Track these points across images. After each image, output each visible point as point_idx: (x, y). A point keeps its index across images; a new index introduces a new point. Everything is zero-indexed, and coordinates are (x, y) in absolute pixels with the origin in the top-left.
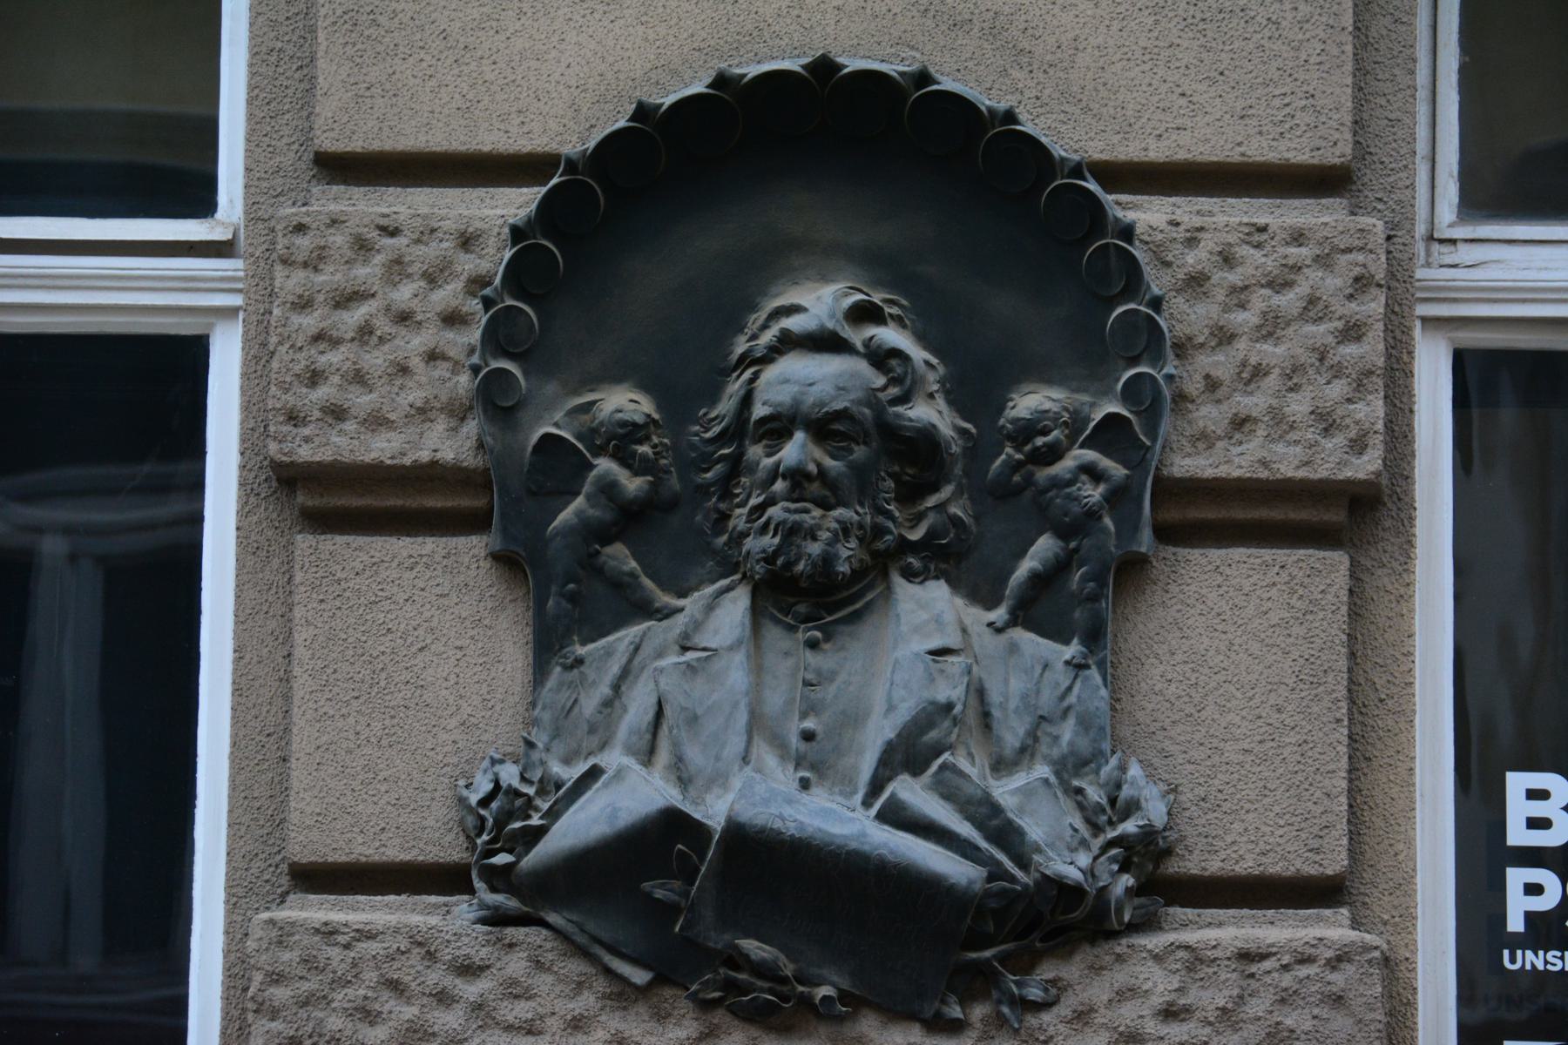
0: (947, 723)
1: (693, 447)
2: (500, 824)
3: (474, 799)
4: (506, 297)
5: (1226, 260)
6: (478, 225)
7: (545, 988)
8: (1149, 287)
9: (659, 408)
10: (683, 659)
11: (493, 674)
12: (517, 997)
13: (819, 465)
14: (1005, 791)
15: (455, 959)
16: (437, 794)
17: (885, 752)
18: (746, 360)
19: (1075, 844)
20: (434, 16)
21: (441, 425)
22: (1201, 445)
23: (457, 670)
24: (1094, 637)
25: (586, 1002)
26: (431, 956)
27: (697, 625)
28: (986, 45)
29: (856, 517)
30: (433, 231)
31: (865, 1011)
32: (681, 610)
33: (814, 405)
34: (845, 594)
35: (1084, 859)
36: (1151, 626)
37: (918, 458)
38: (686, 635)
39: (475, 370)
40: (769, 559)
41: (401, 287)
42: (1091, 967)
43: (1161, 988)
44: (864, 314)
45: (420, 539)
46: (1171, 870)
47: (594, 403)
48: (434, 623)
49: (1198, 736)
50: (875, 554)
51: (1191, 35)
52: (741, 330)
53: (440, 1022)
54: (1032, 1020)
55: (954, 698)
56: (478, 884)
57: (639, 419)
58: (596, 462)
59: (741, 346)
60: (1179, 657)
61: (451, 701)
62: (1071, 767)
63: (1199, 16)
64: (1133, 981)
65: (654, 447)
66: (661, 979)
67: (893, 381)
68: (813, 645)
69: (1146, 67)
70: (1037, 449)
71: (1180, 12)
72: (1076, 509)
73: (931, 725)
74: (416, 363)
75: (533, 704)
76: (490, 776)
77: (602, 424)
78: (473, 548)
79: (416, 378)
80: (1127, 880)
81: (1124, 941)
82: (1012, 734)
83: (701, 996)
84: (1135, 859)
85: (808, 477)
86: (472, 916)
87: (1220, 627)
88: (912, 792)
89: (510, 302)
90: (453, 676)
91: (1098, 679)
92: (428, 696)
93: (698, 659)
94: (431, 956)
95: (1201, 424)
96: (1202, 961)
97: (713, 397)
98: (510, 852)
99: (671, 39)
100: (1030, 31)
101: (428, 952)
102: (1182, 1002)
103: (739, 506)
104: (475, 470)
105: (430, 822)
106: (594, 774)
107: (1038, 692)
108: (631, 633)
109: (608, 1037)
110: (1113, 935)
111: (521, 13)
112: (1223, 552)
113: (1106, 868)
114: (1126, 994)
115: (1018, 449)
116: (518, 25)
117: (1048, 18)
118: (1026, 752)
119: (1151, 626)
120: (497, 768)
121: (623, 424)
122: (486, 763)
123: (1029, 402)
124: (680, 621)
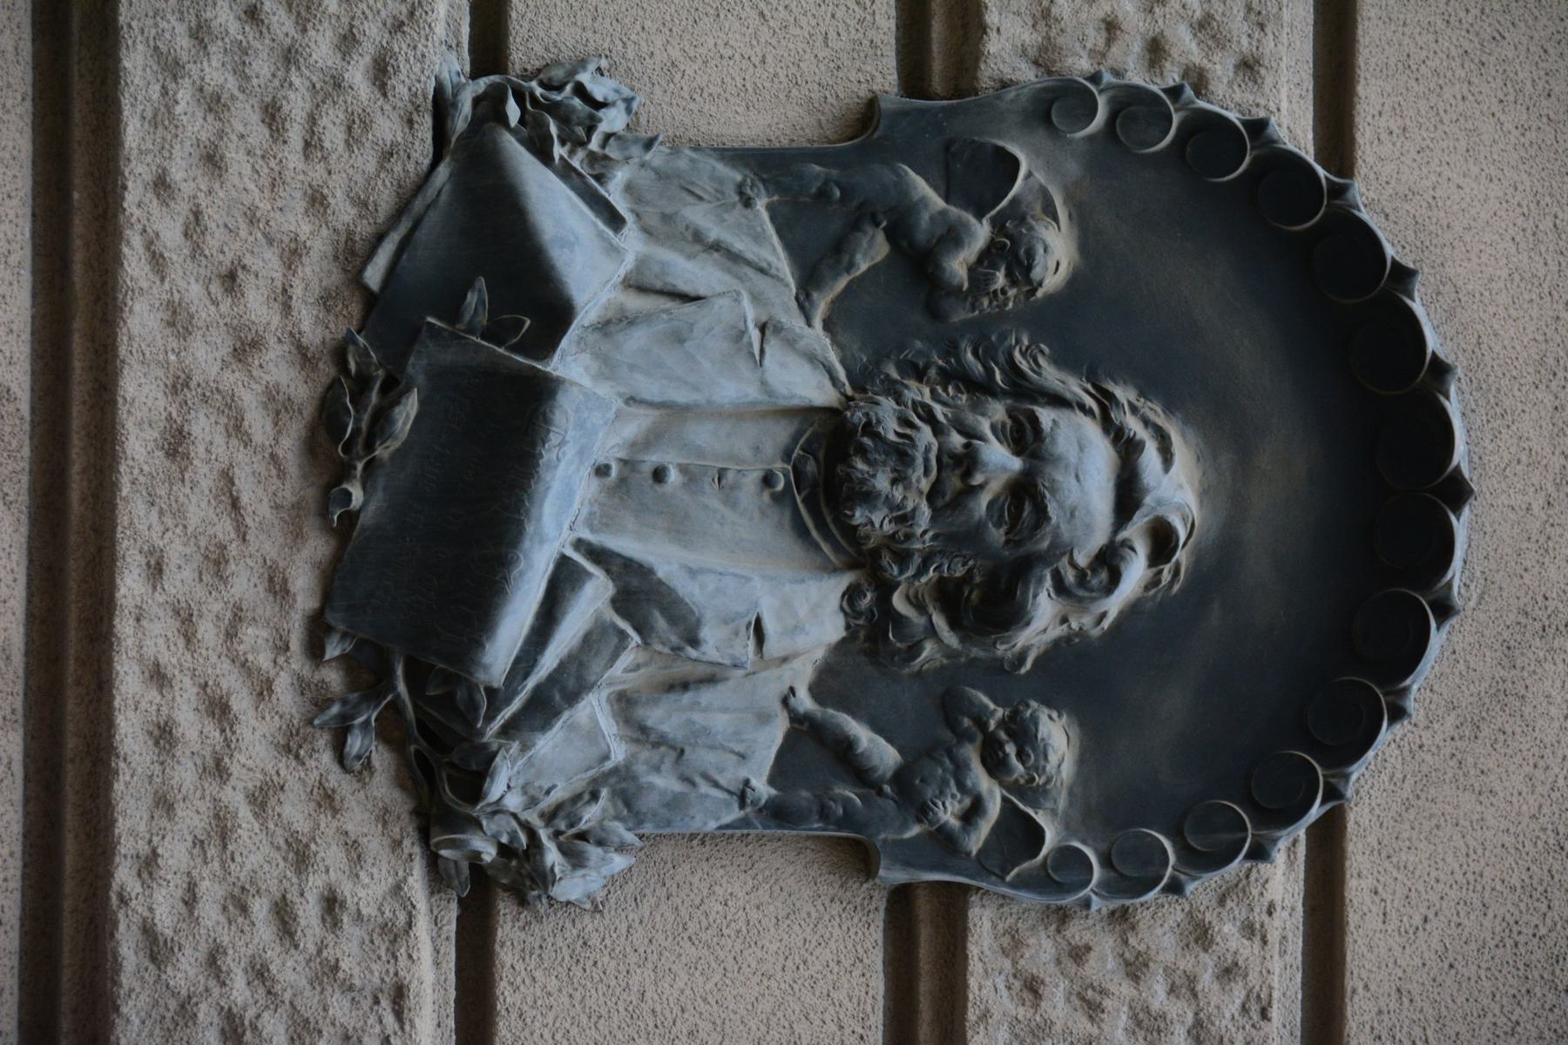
0: (674, 639)
1: (1003, 337)
2: (554, 109)
3: (584, 78)
5: (1227, 971)
6: (1269, 80)
7: (359, 162)
8: (1194, 879)
9: (1050, 298)
10: (751, 325)
12: (349, 129)
13: (981, 487)
14: (594, 709)
15: (394, 55)
16: (589, 34)
17: (641, 566)
18: (1106, 400)
19: (532, 792)
21: (1030, 38)
22: (1006, 941)
23: (737, 57)
24: (779, 814)
26: (398, 27)
27: (790, 343)
28: (1485, 685)
29: (919, 531)
30: (1262, 26)
31: (333, 542)
34: (829, 519)
35: (514, 802)
36: (791, 881)
37: (989, 603)
38: (778, 329)
39: (1095, 78)
40: (870, 428)
42: (386, 810)
43: (362, 893)
44: (1162, 541)
45: (893, 13)
46: (501, 905)
47: (1056, 219)
48: (794, 30)
49: (660, 937)
50: (875, 554)
51: (1498, 929)
54: (323, 740)
55: (704, 648)
56: (483, 83)
57: (1036, 273)
59: (1124, 393)
60: (754, 915)
61: (700, 50)
62: (623, 787)
63: (1522, 939)
64: (370, 861)
65: (1003, 292)
66: (370, 300)
68: (768, 480)
69: (1459, 877)
70: (1001, 745)
71: (1525, 917)
73: (673, 620)
75: (697, 148)
76: (611, 97)
77: (1031, 229)
78: (884, 76)
80: (489, 853)
81: (417, 850)
82: (664, 717)
83: (351, 348)
85: (967, 474)
86: (445, 76)
87: (789, 963)
88: (593, 599)
89: (1176, 119)
90: (730, 53)
91: (728, 819)
92: (706, 22)
93: (750, 344)
94: (398, 27)
95: (1032, 941)
98: (522, 121)
99: (1492, 310)
100: (1501, 737)
102: (345, 919)
104: (975, 78)
105: (557, 26)
106: (614, 220)
107: (712, 747)
108: (781, 262)
109: (302, 238)
110: (424, 835)
111: (1525, 130)
112: (880, 967)
113: (502, 828)
115: (1002, 723)
117: (1518, 759)
118: (641, 733)
119: (791, 881)
120: (621, 106)
121: (1030, 255)
122: (627, 92)
123: (1058, 737)
124: (795, 321)
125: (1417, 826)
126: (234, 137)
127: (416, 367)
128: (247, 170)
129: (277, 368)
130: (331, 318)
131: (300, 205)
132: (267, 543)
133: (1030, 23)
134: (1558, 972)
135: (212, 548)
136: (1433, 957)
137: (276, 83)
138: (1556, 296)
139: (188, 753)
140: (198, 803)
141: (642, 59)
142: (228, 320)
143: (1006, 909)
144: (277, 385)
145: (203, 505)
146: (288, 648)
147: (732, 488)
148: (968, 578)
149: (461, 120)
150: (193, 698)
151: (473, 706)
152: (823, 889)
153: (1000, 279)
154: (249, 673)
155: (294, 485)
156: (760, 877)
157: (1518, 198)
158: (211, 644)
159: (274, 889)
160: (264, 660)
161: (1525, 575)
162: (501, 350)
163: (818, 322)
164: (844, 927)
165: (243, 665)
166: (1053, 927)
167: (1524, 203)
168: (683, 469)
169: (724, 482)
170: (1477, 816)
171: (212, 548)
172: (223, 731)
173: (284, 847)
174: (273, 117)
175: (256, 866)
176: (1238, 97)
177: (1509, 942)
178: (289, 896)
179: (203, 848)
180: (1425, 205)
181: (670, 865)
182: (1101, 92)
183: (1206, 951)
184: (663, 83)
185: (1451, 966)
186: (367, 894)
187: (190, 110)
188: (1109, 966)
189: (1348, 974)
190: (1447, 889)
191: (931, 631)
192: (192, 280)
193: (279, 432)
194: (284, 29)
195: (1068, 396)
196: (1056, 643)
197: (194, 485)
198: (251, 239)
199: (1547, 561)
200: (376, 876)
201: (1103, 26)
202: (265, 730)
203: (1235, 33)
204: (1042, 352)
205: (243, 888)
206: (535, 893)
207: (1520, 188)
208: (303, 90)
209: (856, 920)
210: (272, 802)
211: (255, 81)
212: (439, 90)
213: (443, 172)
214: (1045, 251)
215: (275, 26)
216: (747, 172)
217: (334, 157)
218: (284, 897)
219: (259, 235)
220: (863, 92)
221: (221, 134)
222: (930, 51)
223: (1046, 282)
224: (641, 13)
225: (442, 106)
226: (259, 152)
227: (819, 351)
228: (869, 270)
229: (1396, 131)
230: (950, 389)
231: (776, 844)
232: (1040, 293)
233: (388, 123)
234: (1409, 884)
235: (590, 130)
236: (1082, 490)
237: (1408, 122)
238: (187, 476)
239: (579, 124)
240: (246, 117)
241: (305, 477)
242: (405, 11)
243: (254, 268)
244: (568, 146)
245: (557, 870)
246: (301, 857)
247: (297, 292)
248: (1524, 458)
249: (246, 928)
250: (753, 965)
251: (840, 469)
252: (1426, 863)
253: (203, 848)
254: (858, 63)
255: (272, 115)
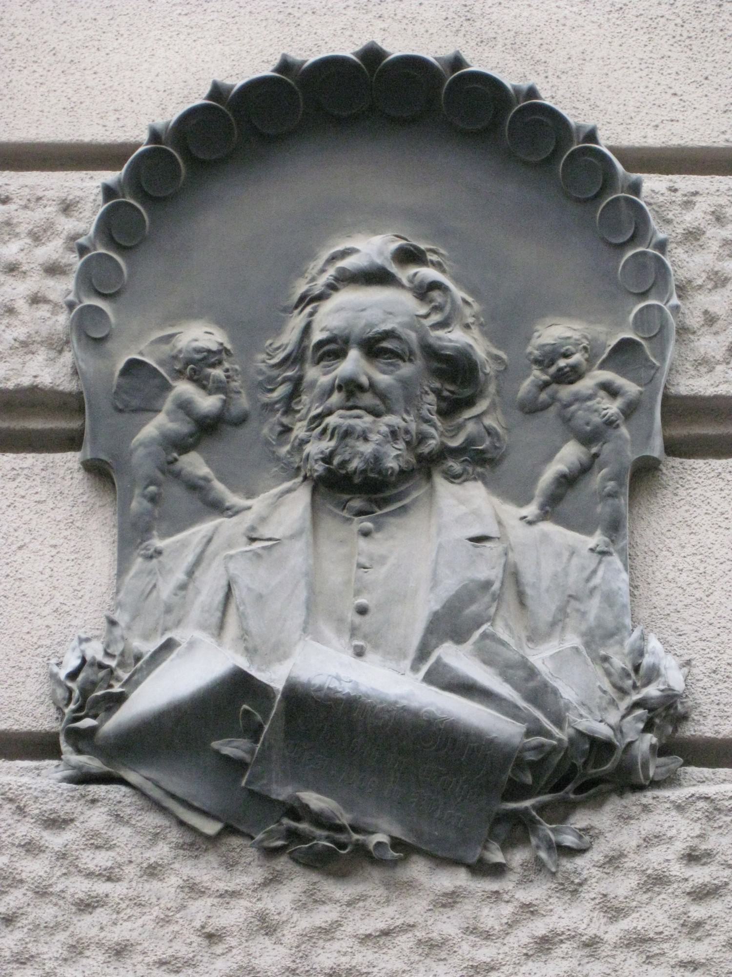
0: (487, 599)
1: (260, 372)
2: (85, 692)
3: (63, 674)
4: (98, 246)
5: (718, 219)
6: (78, 193)
7: (123, 839)
8: (654, 233)
9: (232, 339)
10: (248, 548)
11: (83, 569)
12: (98, 847)
13: (370, 379)
14: (541, 657)
15: (42, 813)
16: (31, 672)
17: (431, 622)
18: (306, 300)
19: (604, 704)
20: (46, 38)
21: (42, 355)
22: (703, 369)
23: (51, 565)
24: (614, 527)
25: (162, 851)
26: (21, 811)
27: (263, 520)
28: (508, 57)
29: (403, 424)
30: (39, 199)
31: (415, 858)
32: (249, 508)
33: (366, 325)
34: (395, 491)
35: (613, 717)
36: (663, 524)
37: (457, 377)
38: (253, 529)
39: (71, 306)
40: (327, 459)
41: (10, 245)
42: (620, 817)
43: (684, 835)
44: (409, 256)
45: (22, 455)
46: (688, 734)
47: (172, 336)
48: (33, 525)
49: (708, 617)
50: (420, 458)
51: (679, 49)
52: (302, 275)
53: (28, 869)
54: (567, 865)
55: (493, 578)
56: (65, 747)
57: (214, 347)
58: (174, 384)
59: (301, 287)
60: (689, 550)
61: (45, 592)
62: (598, 638)
63: (685, 34)
64: (659, 829)
65: (227, 370)
66: (229, 830)
67: (437, 309)
68: (366, 534)
69: (644, 74)
70: (560, 369)
71: (670, 31)
72: (596, 419)
73: (472, 600)
74: (21, 305)
75: (118, 592)
76: (78, 653)
77: (180, 351)
78: (69, 461)
79: (21, 317)
80: (650, 739)
81: (649, 794)
82: (544, 608)
83: (266, 844)
84: (657, 721)
85: (361, 388)
86: (59, 775)
87: (724, 525)
88: (459, 659)
89: (101, 250)
90: (48, 570)
91: (619, 564)
92: (25, 587)
93: (264, 548)
94: (21, 811)
95: (702, 351)
96: (719, 810)
97: (278, 328)
98: (95, 717)
99: (244, 54)
100: (545, 47)
101: (18, 807)
102: (703, 847)
103: (300, 420)
104: (70, 394)
105: (24, 696)
106: (168, 646)
107: (566, 575)
108: (204, 528)
109: (181, 882)
110: (638, 788)
111: (119, 35)
112: (723, 461)
113: (633, 726)
114: (650, 841)
115: (543, 371)
116: (116, 44)
117: (560, 36)
118: (557, 623)
119: (663, 524)
120: (84, 646)
121: (198, 351)
122: (75, 642)
123: (552, 332)
124: (248, 519)
125: (610, 100)
126: (102, 935)
127: (282, 792)
128: (129, 925)
129: (282, 900)
130: (243, 860)
131: (155, 885)
132: (417, 908)
133: (31, 356)
134: (707, 12)
135: (420, 951)
136: (700, 90)
137: (61, 902)
138: (235, 14)
139: (580, 968)
140: (618, 961)
141: (51, 634)
142: (243, 939)
143: (679, 369)
144: (294, 901)
145: (386, 958)
146: (497, 892)
147: (372, 559)
148: (437, 393)
149: (92, 763)
150: (537, 965)
151: (539, 748)
152: (667, 501)
153: (218, 372)
154: (516, 922)
155: (369, 885)
156: (660, 546)
157: (166, 38)
158: (495, 951)
159: (683, 902)
160: (507, 910)
161: (430, 32)
162: (266, 727)
163: (249, 503)
164: (695, 486)
165: (510, 926)
166: (692, 337)
167: (170, 34)
168: (358, 593)
169: (367, 565)
170: (601, 62)
171: (420, 951)
172: (562, 942)
173: (650, 894)
174: (88, 905)
175: (665, 915)
176: (87, 214)
177: (688, 42)
178: (688, 890)
179: (653, 956)
180: (169, 97)
181: (654, 611)
182: (81, 302)
183: (704, 233)
184: (69, 618)
185: (706, 78)
186: (683, 830)
187: (81, 968)
188: (719, 298)
189: (715, 145)
190: (653, 81)
191: (478, 417)
192: (213, 967)
193: (330, 900)
194: (20, 896)
195: (303, 324)
196: (485, 334)
197: (372, 965)
198: (181, 921)
199: (420, 18)
200: (670, 824)
201: (35, 306)
202: (560, 909)
203: (43, 216)
204: (271, 345)
205: (683, 925)
206: (680, 707)
207: (159, 37)
208: (67, 883)
209: (689, 478)
210: (615, 903)
211: (60, 919)
212: (71, 780)
213: (132, 777)
214: (196, 340)
215: (17, 903)
216: (135, 554)
217: (119, 859)
218: (689, 894)
219: (178, 916)
220: (80, 475)
221: (100, 945)
222: (52, 429)
223: (220, 341)
224: (16, 635)
225: (84, 778)
226: (114, 916)
227: (270, 501)
228: (210, 466)
229: (117, 116)
230: (298, 408)
231: (636, 535)
232: (229, 346)
233: (94, 818)
234: (650, 105)
235: (101, 666)
236: (371, 307)
237: (112, 108)
238: (365, 971)
239: (97, 675)
240: (86, 926)
241: (365, 880)
242: (9, 806)
243: (203, 919)
244: (113, 682)
245: (662, 687)
246: (657, 881)
247: (222, 886)
248: (348, 33)
249: (713, 922)
250: (726, 550)
251: (357, 480)
252: (634, 94)
253: (653, 956)
254: (59, 480)
255: (86, 906)
